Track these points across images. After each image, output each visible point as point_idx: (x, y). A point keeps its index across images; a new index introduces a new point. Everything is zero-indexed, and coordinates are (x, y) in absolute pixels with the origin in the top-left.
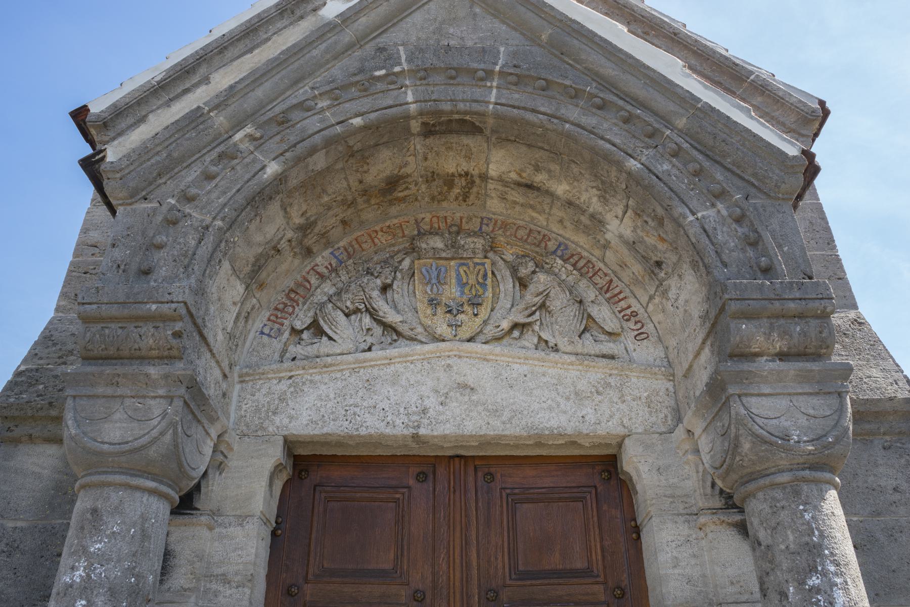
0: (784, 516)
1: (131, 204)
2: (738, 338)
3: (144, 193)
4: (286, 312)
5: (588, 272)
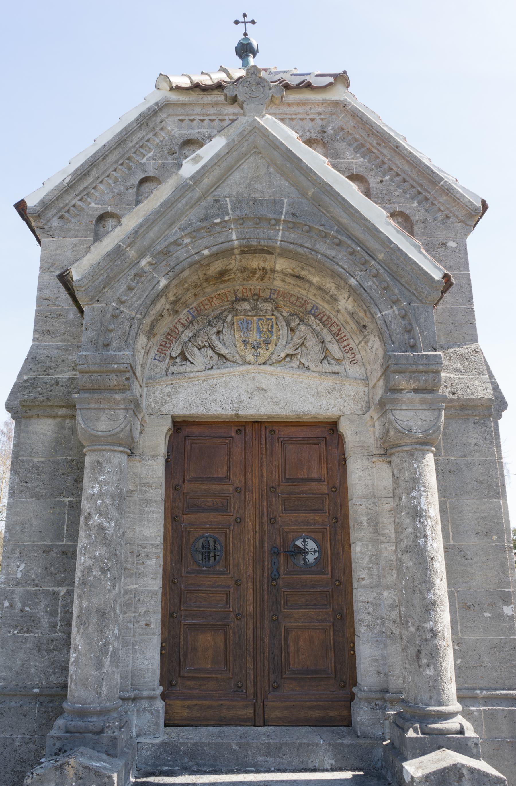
0: (405, 465)
1: (91, 304)
2: (393, 383)
3: (97, 298)
4: (167, 347)
5: (328, 324)
